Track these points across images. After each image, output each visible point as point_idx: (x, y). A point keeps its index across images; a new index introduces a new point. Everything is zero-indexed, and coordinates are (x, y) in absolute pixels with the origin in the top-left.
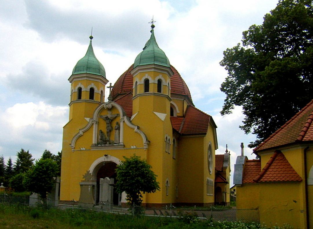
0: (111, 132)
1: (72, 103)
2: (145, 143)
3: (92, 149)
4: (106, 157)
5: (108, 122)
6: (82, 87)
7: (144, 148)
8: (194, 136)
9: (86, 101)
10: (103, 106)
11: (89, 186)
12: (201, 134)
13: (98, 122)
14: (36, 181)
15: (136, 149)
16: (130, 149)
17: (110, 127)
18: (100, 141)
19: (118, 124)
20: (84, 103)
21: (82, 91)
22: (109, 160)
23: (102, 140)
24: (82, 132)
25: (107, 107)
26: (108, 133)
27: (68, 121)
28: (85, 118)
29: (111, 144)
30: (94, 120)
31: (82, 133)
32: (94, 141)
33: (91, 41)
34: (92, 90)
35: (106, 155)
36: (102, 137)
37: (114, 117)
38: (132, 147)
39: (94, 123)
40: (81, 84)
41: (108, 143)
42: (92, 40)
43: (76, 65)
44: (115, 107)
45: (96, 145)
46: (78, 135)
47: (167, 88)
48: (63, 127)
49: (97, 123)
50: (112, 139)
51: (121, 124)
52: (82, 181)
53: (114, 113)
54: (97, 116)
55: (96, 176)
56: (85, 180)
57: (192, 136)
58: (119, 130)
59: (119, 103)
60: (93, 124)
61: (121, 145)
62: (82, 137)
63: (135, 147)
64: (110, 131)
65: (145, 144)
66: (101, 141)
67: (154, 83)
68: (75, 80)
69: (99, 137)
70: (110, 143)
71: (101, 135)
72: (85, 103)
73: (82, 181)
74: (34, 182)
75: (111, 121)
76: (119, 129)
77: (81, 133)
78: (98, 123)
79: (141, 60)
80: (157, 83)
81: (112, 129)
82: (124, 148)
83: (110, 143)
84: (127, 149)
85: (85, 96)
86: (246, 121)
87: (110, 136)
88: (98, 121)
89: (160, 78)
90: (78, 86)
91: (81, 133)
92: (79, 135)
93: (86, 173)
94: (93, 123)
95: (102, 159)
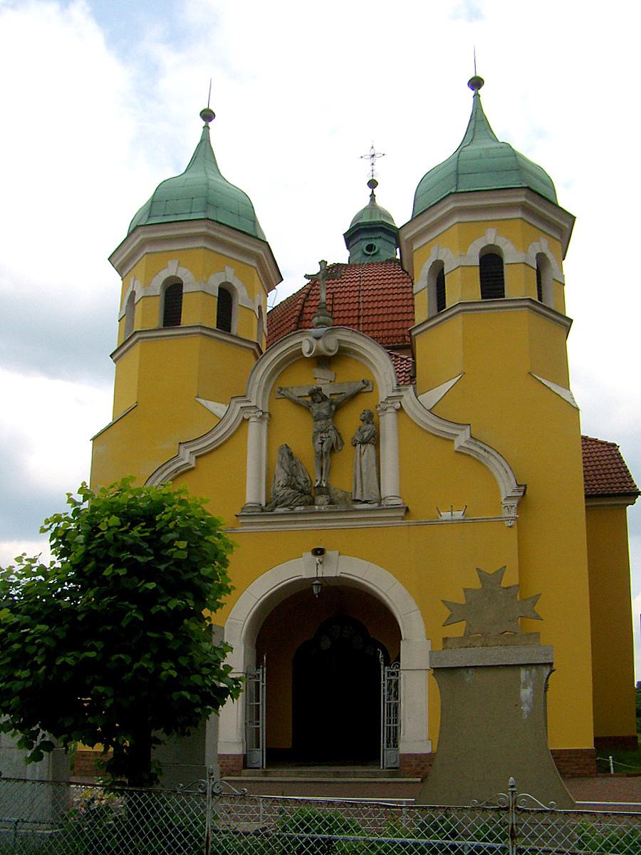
0: (336, 455)
1: (137, 341)
2: (508, 498)
3: (240, 529)
4: (317, 559)
5: (325, 412)
6: (186, 276)
7: (501, 520)
8: (605, 503)
9: (205, 332)
10: (298, 348)
11: (523, 673)
12: (619, 495)
13: (270, 415)
14: (100, 645)
15: (463, 521)
16: (436, 522)
17: (332, 434)
18: (282, 492)
19: (369, 418)
20: (197, 342)
21: (184, 292)
22: (330, 571)
23: (293, 487)
24: (182, 460)
25: (318, 350)
26: (321, 456)
27: (108, 419)
28: (199, 400)
29: (344, 504)
30: (253, 404)
31: (181, 456)
32: (253, 493)
33: (206, 128)
34: (225, 297)
35: (319, 552)
36: (292, 474)
37: (348, 391)
38: (446, 515)
39: (253, 417)
40: (179, 265)
41: (321, 499)
42: (210, 124)
43: (154, 194)
44: (356, 353)
45: (269, 507)
46: (174, 467)
47: (255, 322)
48: (94, 439)
49: (267, 416)
50: (342, 482)
51: (388, 423)
52: (445, 640)
53: (347, 378)
54: (265, 390)
55: (254, 645)
56: (468, 634)
57: (605, 503)
58: (377, 446)
59: (376, 334)
60: (245, 421)
61: (395, 508)
62: (192, 473)
63: (458, 515)
64: (332, 449)
65: (510, 503)
66: (290, 491)
67: (525, 263)
68: (147, 250)
69: (281, 477)
70: (331, 502)
71: (286, 467)
72: (199, 339)
73: (445, 640)
74: (92, 654)
75: (333, 407)
76: (374, 439)
77: (187, 457)
78: (268, 418)
79: (460, 177)
80: (217, 295)
81: (339, 442)
82: (403, 518)
83: (331, 502)
84: (418, 524)
85: (198, 311)
86: (47, 631)
87: (329, 473)
88: (266, 410)
89: (544, 251)
90: (164, 275)
91: (187, 457)
92: (178, 468)
93: (477, 585)
94: (246, 417)
95: (301, 568)
